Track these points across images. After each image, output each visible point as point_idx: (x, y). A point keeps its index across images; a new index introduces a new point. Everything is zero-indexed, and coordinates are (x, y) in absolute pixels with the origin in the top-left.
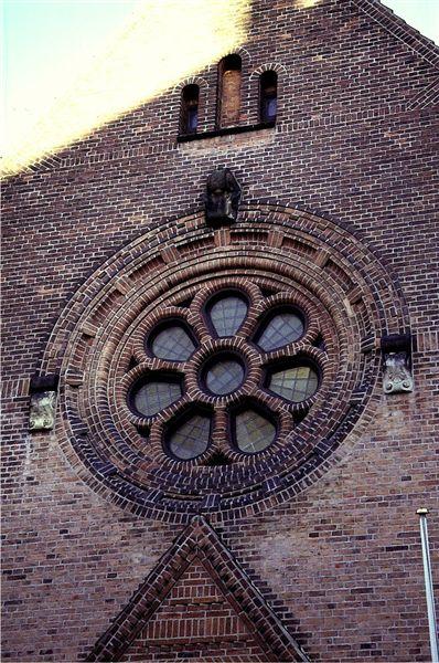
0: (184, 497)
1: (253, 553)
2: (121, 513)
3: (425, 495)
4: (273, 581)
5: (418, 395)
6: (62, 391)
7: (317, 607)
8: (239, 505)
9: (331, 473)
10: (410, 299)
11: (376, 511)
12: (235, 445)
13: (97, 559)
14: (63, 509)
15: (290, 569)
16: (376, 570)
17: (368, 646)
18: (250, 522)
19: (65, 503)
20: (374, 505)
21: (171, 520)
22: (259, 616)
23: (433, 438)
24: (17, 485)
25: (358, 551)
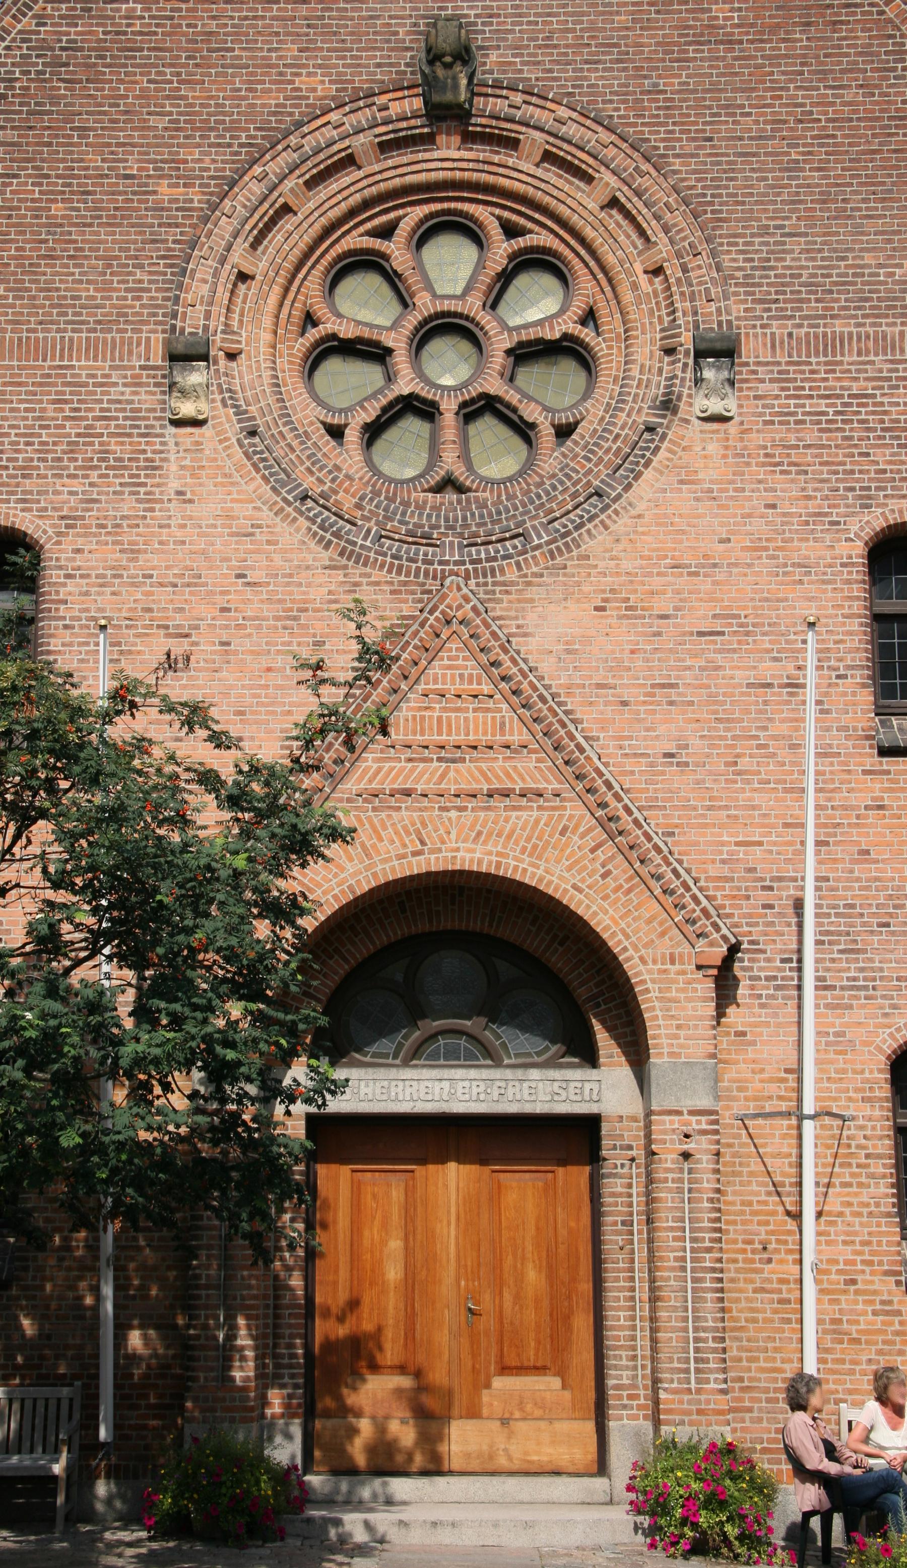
0: (410, 539)
1: (518, 627)
2: (325, 556)
3: (749, 565)
4: (546, 666)
5: (742, 423)
6: (216, 363)
7: (606, 704)
8: (495, 559)
9: (621, 525)
10: (732, 277)
11: (683, 581)
12: (470, 467)
13: (295, 618)
14: (237, 543)
15: (568, 652)
16: (684, 660)
17: (672, 755)
18: (512, 583)
19: (237, 534)
20: (681, 575)
21: (399, 573)
22: (546, 717)
23: (761, 486)
24: (161, 501)
25: (659, 634)
